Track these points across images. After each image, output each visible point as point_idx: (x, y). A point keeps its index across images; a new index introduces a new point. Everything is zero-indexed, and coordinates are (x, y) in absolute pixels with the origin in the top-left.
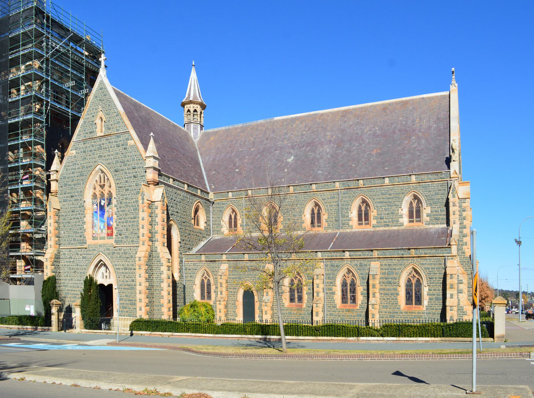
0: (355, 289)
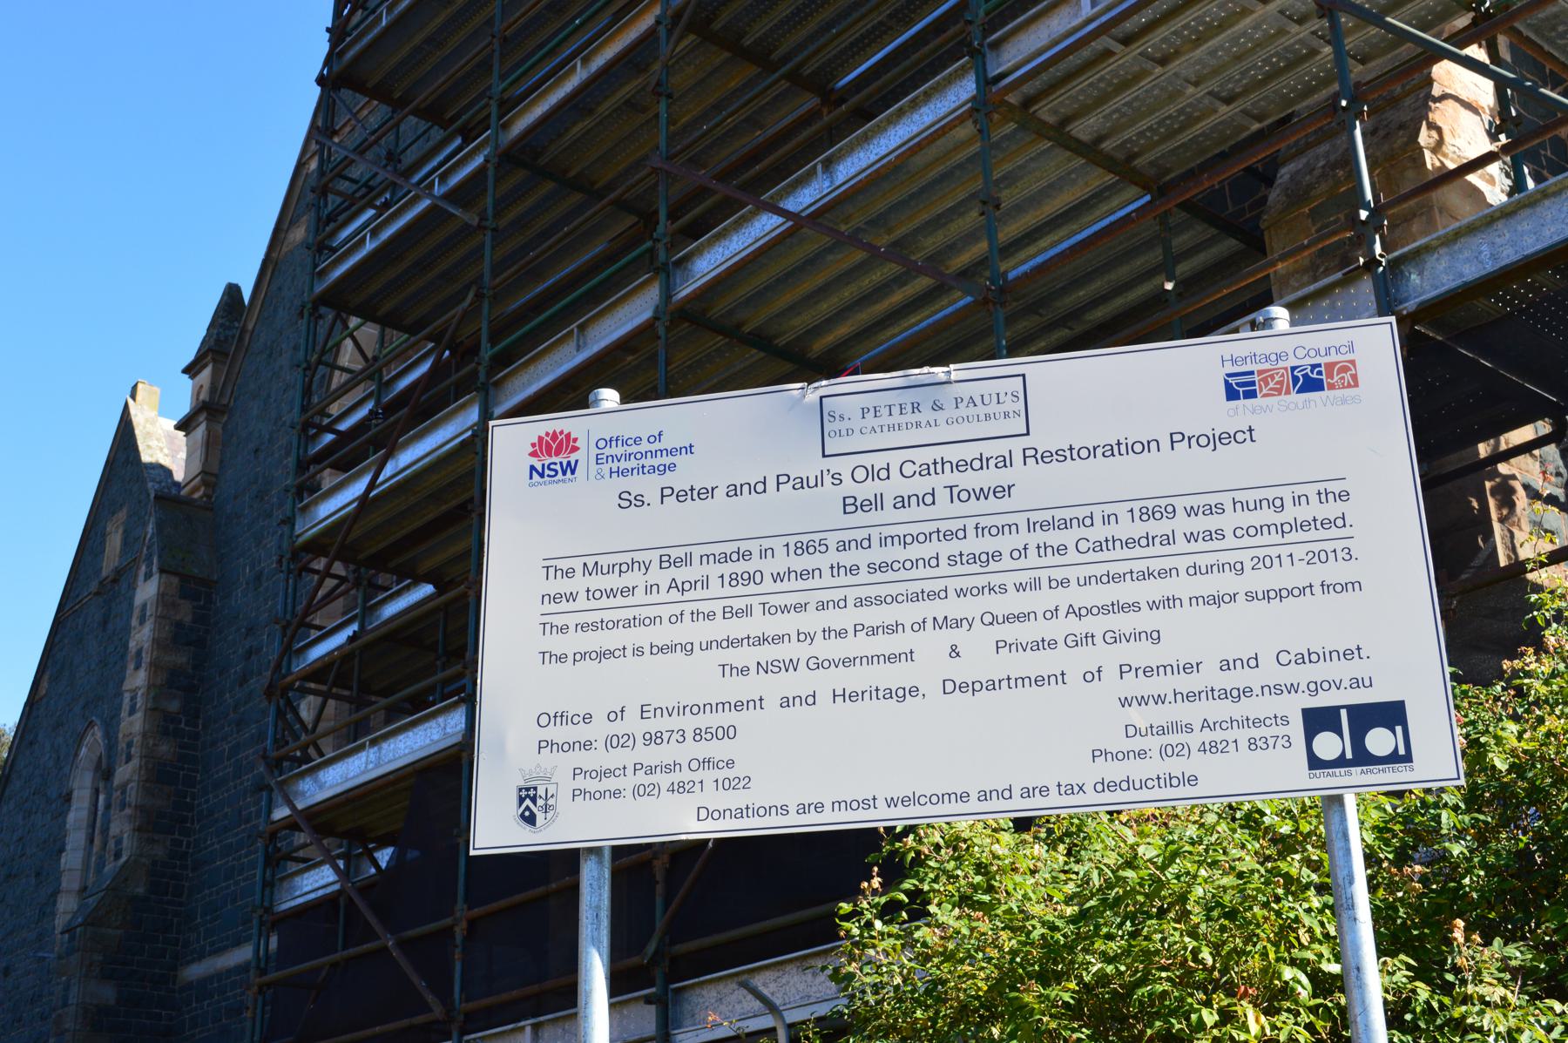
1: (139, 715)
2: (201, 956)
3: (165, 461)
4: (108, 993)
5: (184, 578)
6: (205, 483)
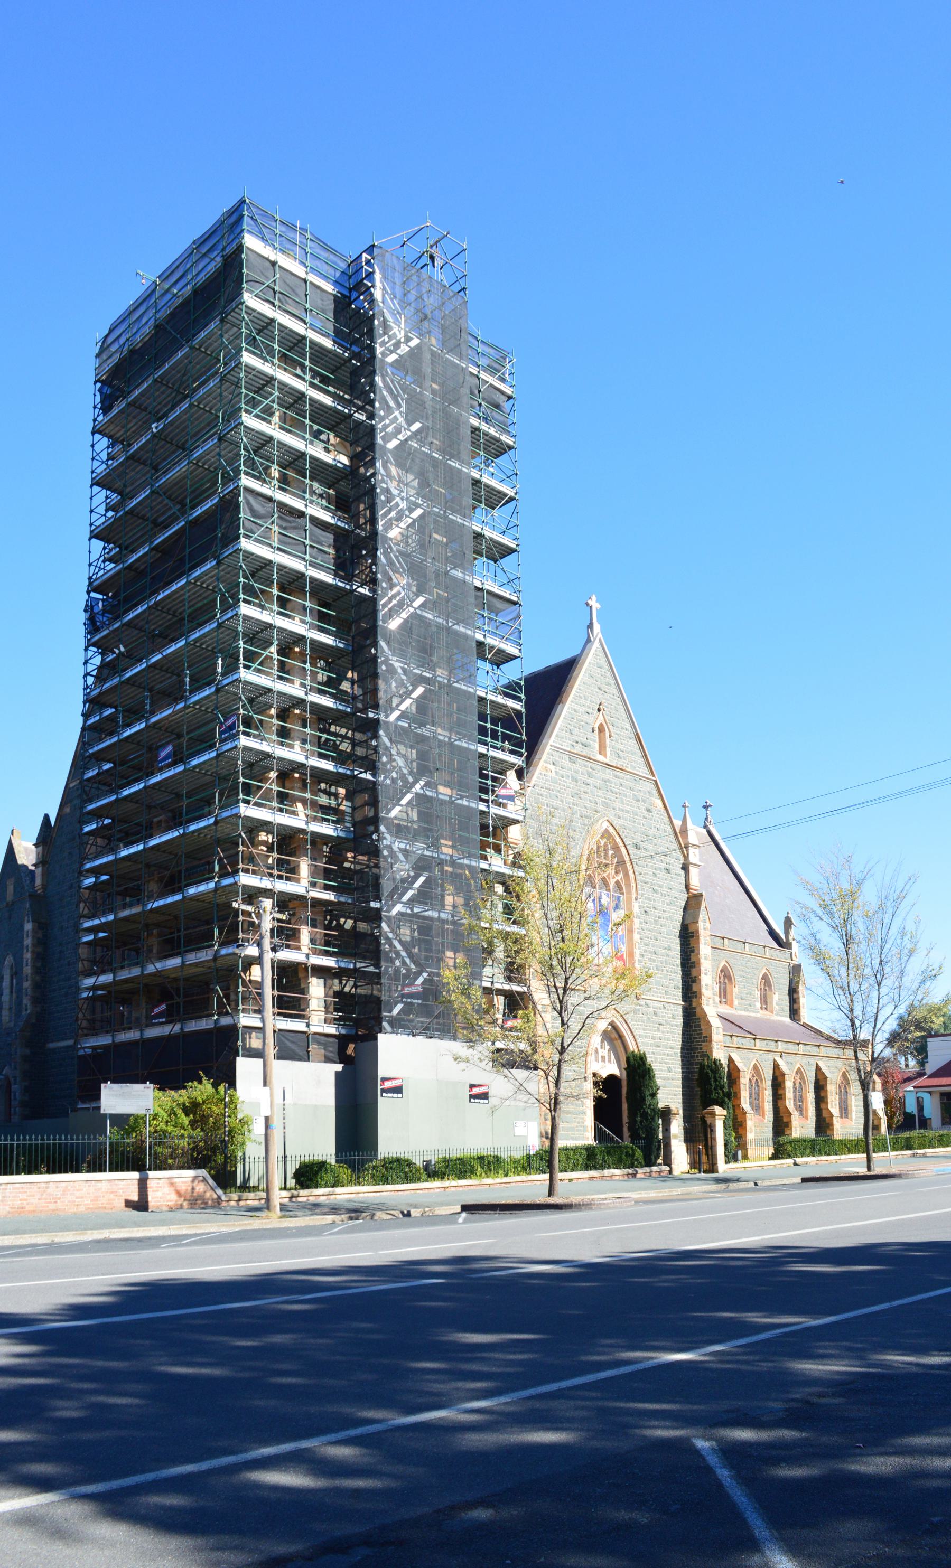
0: (801, 1096)
1: (29, 967)
2: (52, 1042)
3: (26, 863)
4: (27, 1051)
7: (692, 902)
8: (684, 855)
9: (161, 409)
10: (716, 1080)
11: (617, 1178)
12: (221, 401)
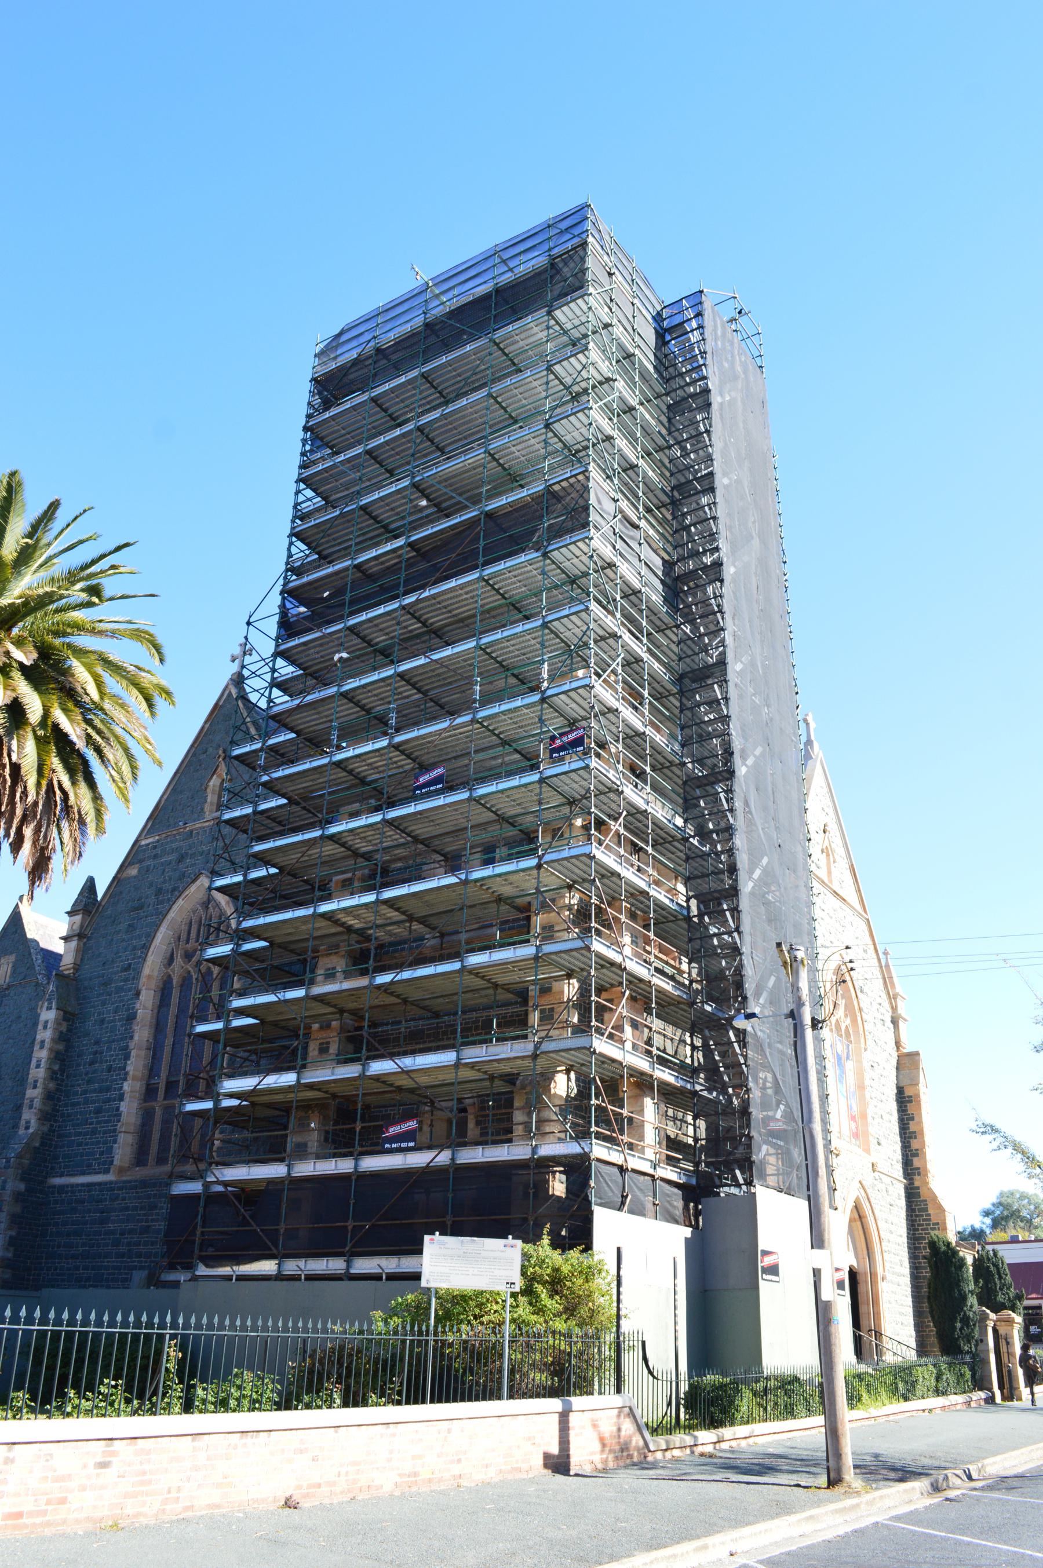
2: (61, 1175)
4: (22, 1187)
5: (65, 1012)
6: (74, 968)
7: (906, 1061)
8: (892, 1008)
9: (405, 413)
10: (1000, 1278)
11: (959, 1407)
12: (546, 390)
